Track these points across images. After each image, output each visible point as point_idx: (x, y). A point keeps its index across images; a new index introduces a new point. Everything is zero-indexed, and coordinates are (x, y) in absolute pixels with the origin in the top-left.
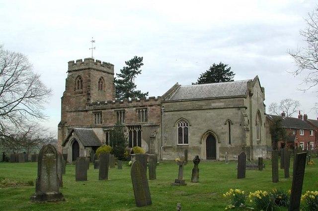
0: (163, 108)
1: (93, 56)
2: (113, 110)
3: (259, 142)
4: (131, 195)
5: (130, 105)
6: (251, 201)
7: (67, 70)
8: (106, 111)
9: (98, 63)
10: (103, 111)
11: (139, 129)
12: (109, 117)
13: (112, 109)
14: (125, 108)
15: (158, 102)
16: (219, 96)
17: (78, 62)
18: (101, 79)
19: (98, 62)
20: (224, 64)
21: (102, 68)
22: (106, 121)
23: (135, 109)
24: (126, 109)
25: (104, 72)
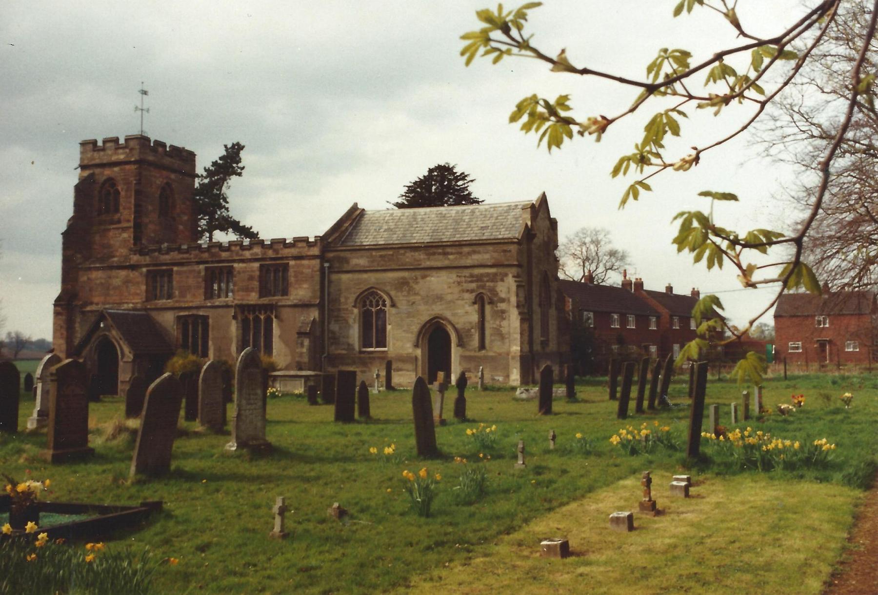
0: (326, 265)
1: (143, 129)
2: (202, 267)
3: (544, 344)
4: (758, 83)
5: (247, 254)
6: (150, 208)
7: (77, 162)
8: (185, 268)
9: (160, 149)
10: (175, 269)
11: (268, 313)
12: (191, 281)
13: (198, 263)
14: (234, 261)
15: (316, 251)
16: (458, 238)
17: (108, 145)
18: (167, 188)
19: (160, 144)
20: (527, 17)
21: (167, 161)
22: (183, 295)
23: (256, 265)
24: (236, 265)
25: (174, 171)
